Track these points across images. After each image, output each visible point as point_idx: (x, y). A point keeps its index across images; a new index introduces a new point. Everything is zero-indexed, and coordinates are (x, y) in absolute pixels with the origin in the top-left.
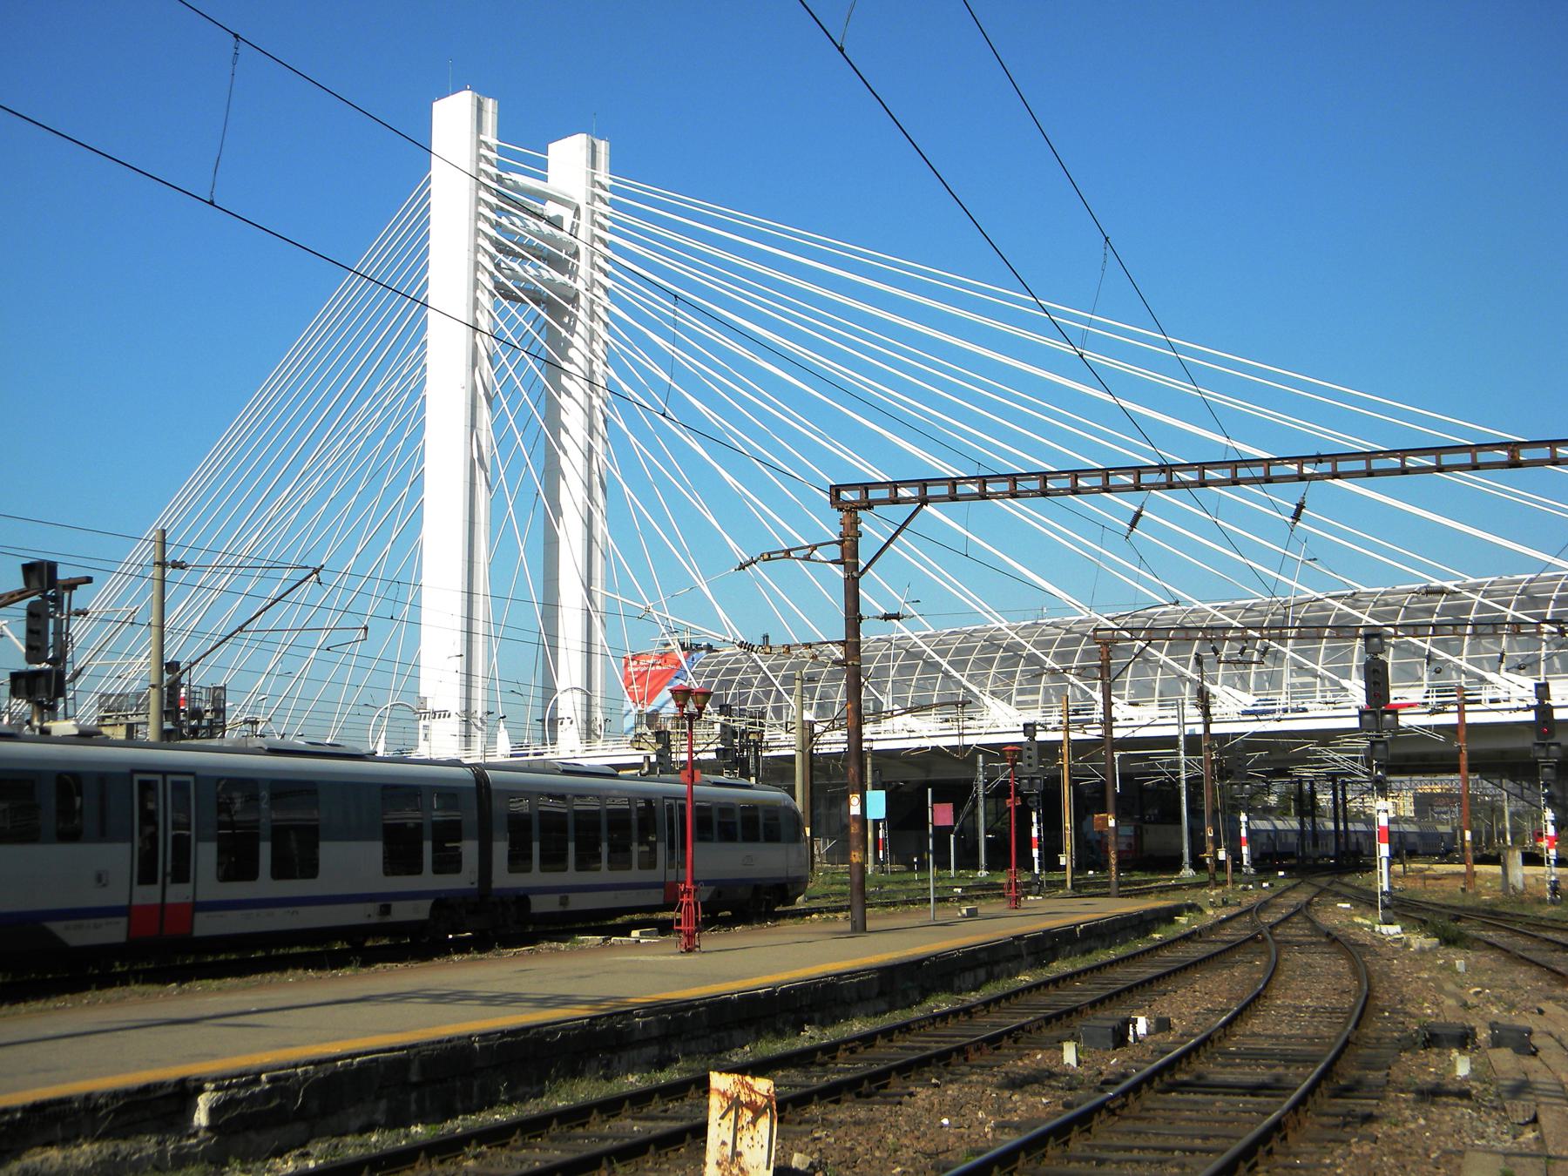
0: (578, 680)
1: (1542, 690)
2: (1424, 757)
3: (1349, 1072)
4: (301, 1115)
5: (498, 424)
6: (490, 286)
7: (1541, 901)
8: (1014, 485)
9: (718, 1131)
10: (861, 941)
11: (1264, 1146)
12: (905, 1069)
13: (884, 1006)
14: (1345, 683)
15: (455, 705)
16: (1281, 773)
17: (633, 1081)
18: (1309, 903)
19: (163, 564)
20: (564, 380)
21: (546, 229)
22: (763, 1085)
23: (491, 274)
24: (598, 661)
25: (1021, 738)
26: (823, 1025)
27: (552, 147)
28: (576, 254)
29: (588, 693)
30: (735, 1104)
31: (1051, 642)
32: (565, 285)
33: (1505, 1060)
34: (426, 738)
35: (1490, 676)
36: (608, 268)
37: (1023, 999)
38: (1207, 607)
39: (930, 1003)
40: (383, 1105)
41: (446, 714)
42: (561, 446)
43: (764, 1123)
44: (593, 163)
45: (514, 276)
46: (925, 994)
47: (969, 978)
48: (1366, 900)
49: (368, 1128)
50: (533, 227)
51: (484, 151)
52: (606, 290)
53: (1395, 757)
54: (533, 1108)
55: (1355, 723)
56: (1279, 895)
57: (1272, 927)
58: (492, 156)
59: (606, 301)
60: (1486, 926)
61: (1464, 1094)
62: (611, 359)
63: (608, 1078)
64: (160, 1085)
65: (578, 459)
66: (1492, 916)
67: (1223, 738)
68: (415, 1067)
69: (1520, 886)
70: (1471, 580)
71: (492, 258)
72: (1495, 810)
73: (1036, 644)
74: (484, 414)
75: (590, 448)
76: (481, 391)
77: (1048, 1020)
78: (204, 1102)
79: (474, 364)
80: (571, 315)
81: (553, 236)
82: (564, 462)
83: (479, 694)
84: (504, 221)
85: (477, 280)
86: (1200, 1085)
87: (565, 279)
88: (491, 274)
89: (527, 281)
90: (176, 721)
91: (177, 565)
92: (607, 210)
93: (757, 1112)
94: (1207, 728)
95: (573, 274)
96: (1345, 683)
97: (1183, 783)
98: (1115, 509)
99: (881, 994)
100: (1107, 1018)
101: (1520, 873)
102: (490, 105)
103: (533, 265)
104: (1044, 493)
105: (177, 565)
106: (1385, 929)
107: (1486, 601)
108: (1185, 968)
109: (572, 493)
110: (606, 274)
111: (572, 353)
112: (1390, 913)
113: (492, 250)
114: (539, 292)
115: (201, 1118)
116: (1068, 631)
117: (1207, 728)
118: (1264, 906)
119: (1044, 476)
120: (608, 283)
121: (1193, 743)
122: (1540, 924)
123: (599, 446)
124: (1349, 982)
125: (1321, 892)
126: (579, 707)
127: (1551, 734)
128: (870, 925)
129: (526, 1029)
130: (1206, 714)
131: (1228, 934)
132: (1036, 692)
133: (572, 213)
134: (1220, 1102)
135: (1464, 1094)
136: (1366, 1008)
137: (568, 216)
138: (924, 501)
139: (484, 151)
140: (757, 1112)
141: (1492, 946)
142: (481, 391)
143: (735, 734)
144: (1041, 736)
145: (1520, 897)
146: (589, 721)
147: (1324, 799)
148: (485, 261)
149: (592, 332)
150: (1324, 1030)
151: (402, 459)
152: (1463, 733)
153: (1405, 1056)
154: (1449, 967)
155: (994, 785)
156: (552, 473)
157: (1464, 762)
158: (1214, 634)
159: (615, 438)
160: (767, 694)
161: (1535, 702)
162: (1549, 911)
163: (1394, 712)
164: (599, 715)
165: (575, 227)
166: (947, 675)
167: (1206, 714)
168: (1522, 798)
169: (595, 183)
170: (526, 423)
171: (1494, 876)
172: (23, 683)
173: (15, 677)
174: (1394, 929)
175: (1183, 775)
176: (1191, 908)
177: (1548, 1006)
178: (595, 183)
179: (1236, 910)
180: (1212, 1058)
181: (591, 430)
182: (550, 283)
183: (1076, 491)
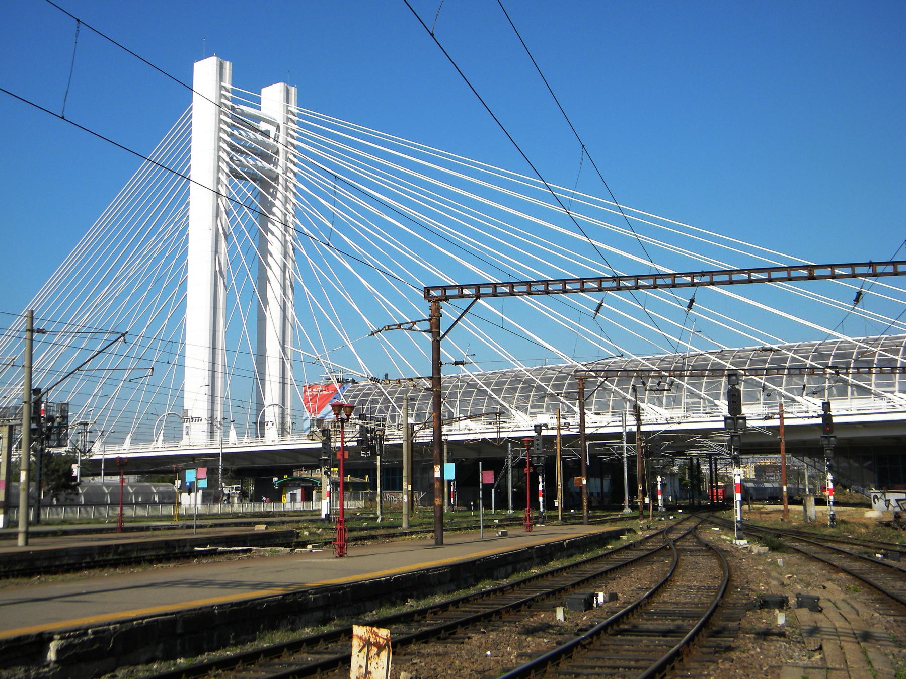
0: (277, 400)
1: (826, 406)
2: (761, 444)
3: (718, 623)
5: (231, 251)
6: (227, 170)
7: (825, 526)
8: (530, 287)
9: (357, 660)
10: (440, 550)
13: (453, 587)
14: (717, 402)
15: (204, 414)
16: (681, 453)
17: (308, 632)
18: (696, 528)
19: (31, 331)
20: (270, 225)
21: (260, 137)
22: (384, 633)
23: (228, 163)
24: (288, 388)
25: (533, 433)
27: (264, 90)
28: (277, 153)
30: (367, 644)
31: (551, 378)
32: (270, 170)
33: (804, 614)
35: (798, 398)
36: (296, 160)
37: (533, 583)
38: (639, 358)
39: (480, 586)
40: (161, 646)
41: (199, 419)
42: (268, 264)
43: (384, 654)
44: (288, 100)
45: (241, 165)
46: (477, 581)
47: (503, 571)
49: (152, 660)
50: (252, 137)
51: (224, 92)
52: (295, 174)
53: (744, 444)
58: (229, 95)
59: (295, 180)
61: (782, 634)
62: (298, 214)
64: (27, 637)
66: (798, 534)
67: (648, 433)
69: (813, 517)
70: (787, 344)
71: (228, 154)
72: (800, 475)
73: (542, 380)
74: (223, 245)
76: (221, 231)
78: (53, 646)
79: (217, 216)
80: (274, 188)
82: (270, 273)
83: (219, 407)
84: (235, 133)
86: (635, 631)
88: (228, 163)
89: (249, 168)
90: (39, 423)
91: (40, 331)
92: (296, 127)
95: (276, 164)
96: (717, 402)
97: (625, 459)
99: (452, 581)
100: (582, 593)
101: (813, 510)
102: (227, 65)
103: (252, 158)
104: (547, 292)
105: (40, 331)
106: (738, 542)
107: (795, 356)
109: (274, 291)
110: (295, 164)
113: (228, 149)
114: (255, 174)
115: (52, 656)
116: (560, 372)
117: (639, 428)
118: (671, 529)
119: (547, 283)
120: (296, 169)
121: (631, 436)
122: (824, 538)
123: (290, 264)
124: (718, 572)
125: (703, 521)
127: (831, 431)
128: (445, 541)
129: (246, 602)
130: (639, 420)
131: (650, 545)
133: (275, 128)
134: (645, 640)
135: (782, 634)
137: (272, 130)
139: (224, 92)
140: (380, 648)
141: (798, 551)
142: (221, 231)
143: (368, 431)
145: (813, 523)
146: (283, 424)
147: (705, 468)
148: (224, 156)
150: (704, 600)
152: (782, 430)
153: (749, 613)
154: (774, 563)
156: (263, 280)
157: (783, 447)
158: (643, 374)
159: (299, 260)
160: (387, 408)
161: (823, 413)
162: (829, 531)
164: (289, 420)
167: (639, 420)
168: (815, 468)
170: (247, 250)
171: (799, 512)
174: (743, 542)
175: (625, 455)
176: (630, 530)
177: (829, 585)
178: (288, 111)
179: (654, 532)
180: (640, 616)
181: (285, 254)
182: (262, 169)
183: (565, 291)
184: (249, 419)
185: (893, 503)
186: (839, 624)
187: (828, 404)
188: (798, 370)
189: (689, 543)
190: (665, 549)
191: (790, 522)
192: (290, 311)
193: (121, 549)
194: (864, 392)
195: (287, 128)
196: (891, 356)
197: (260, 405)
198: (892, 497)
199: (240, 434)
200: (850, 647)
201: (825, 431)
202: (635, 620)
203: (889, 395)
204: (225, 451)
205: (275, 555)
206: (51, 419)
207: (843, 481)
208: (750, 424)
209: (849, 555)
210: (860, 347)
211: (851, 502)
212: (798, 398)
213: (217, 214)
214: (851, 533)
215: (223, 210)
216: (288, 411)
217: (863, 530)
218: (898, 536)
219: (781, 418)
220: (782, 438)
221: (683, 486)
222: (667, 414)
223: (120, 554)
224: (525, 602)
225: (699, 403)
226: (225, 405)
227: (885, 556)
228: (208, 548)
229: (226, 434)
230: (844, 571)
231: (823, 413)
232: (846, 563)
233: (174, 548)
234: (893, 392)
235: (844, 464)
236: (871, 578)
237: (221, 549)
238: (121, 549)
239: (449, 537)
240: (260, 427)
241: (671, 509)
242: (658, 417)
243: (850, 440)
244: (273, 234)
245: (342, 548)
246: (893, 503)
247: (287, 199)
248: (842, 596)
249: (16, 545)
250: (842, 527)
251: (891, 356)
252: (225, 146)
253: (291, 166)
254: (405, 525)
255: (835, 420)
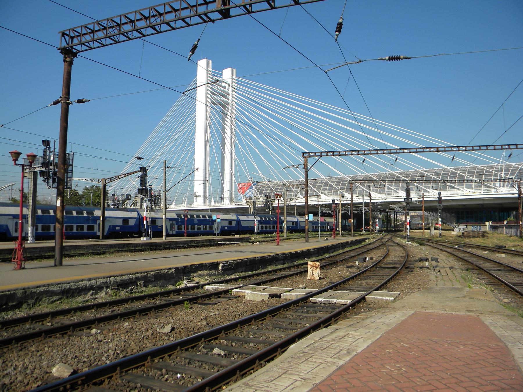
0: (229, 189)
1: (440, 194)
2: (414, 207)
3: (407, 265)
4: (233, 269)
5: (212, 131)
6: (210, 102)
7: (437, 237)
8: (339, 153)
9: (310, 271)
10: (308, 244)
11: (334, 318)
12: (329, 265)
13: (317, 255)
14: (398, 191)
15: (202, 194)
16: (384, 210)
17: (280, 267)
18: (391, 238)
19: (165, 167)
20: (226, 122)
21: (222, 89)
22: (318, 263)
23: (210, 99)
24: (233, 184)
25: (331, 202)
26: (316, 257)
28: (229, 94)
29: (231, 191)
30: (313, 267)
31: (335, 182)
32: (226, 101)
33: (434, 263)
34: (196, 201)
35: (428, 190)
36: (236, 97)
37: (342, 254)
38: (369, 174)
39: (325, 255)
40: (244, 268)
41: (200, 196)
43: (318, 270)
44: (233, 74)
45: (215, 99)
46: (324, 253)
47: (331, 251)
48: (404, 237)
49: (242, 272)
50: (219, 89)
52: (235, 102)
53: (411, 207)
54: (266, 270)
55: (403, 200)
56: (385, 236)
57: (386, 242)
59: (235, 105)
60: (427, 242)
61: (428, 268)
62: (237, 118)
63: (291, 262)
64: (215, 262)
65: (229, 140)
66: (428, 240)
67: (374, 203)
68: (248, 262)
69: (433, 234)
70: (425, 169)
71: (210, 95)
72: (428, 219)
73: (331, 182)
74: (209, 130)
75: (232, 137)
76: (208, 125)
77: (350, 258)
78: (221, 266)
79: (206, 119)
80: (227, 108)
81: (224, 90)
82: (226, 140)
83: (207, 191)
84: (213, 87)
85: (207, 100)
86: (381, 267)
87: (226, 100)
88: (210, 99)
89: (218, 100)
90: (151, 197)
91: (168, 167)
92: (236, 85)
93: (317, 268)
94: (371, 201)
95: (228, 99)
96: (398, 191)
97: (363, 213)
98: (360, 158)
99: (317, 253)
100: (362, 257)
101: (434, 232)
102: (210, 62)
103: (219, 97)
104: (346, 155)
105: (168, 167)
106: (408, 242)
107: (428, 174)
108: (372, 249)
109: (227, 147)
110: (235, 99)
111: (228, 116)
112: (409, 239)
113: (211, 94)
114: (221, 103)
115: (220, 268)
116: (338, 179)
117: (371, 201)
118: (382, 238)
119: (346, 151)
120: (236, 101)
121: (366, 204)
122: (437, 241)
123: (234, 137)
124: (403, 252)
125: (393, 236)
126: (229, 194)
127: (441, 203)
128: (309, 241)
129: (263, 257)
130: (371, 198)
131: (377, 243)
132: (331, 192)
134: (386, 270)
135: (428, 268)
136: (408, 256)
138: (321, 156)
140: (317, 268)
141: (429, 245)
142: (208, 125)
143: (268, 201)
144: (336, 202)
145: (433, 237)
146: (231, 198)
147: (392, 216)
148: (209, 96)
149: (231, 111)
150: (401, 259)
151: (181, 138)
152: (423, 202)
153: (417, 263)
154: (422, 249)
155: (322, 213)
156: (223, 143)
157: (423, 209)
158: (371, 181)
159: (237, 135)
160: (272, 192)
161: (438, 196)
162: (439, 239)
163: (411, 199)
164: (233, 196)
165: (228, 89)
166: (311, 188)
167: (371, 198)
168: (434, 216)
169: (233, 78)
170: (217, 131)
171: (428, 232)
172: (140, 191)
173: (139, 189)
174: (410, 242)
175: (363, 211)
176: (369, 238)
177: (440, 255)
179: (376, 239)
180: (382, 263)
181: (232, 133)
182: (223, 101)
183: (352, 155)
184: (218, 196)
185: (462, 229)
186: (445, 265)
187: (440, 193)
188: (428, 180)
189: (390, 243)
190: (383, 245)
191: (425, 236)
192: (234, 154)
193: (196, 242)
194: (453, 188)
195: (232, 94)
196: (463, 174)
197: (222, 190)
198: (461, 227)
199: (215, 202)
200: (449, 271)
201: (439, 203)
202: (380, 264)
203: (462, 189)
204: (211, 208)
205: (247, 245)
206: (155, 196)
207: (444, 221)
208: (413, 200)
209: (446, 246)
210: (452, 171)
211: (446, 229)
212: (428, 190)
213: (206, 118)
214: (447, 239)
215: (208, 116)
216: (233, 193)
217: (451, 239)
218: (463, 240)
219: (423, 198)
220: (423, 205)
221: (383, 223)
222: (380, 195)
223: (196, 243)
224: (344, 259)
225: (391, 192)
226: (209, 190)
227: (459, 247)
228: (223, 242)
229: (210, 202)
230: (445, 251)
231: (438, 196)
232: (446, 249)
233: (212, 242)
234: (463, 188)
235: (445, 215)
236: (454, 253)
237: (227, 243)
238: (196, 242)
239: (310, 240)
240: (222, 199)
241: (380, 231)
242: (376, 196)
243: (447, 206)
244: (227, 125)
245: (278, 242)
246: (462, 229)
247: (232, 113)
248: (445, 258)
249: (162, 239)
250: (444, 237)
251: (463, 174)
252: (209, 92)
253: (234, 99)
254: (285, 236)
255: (443, 198)
